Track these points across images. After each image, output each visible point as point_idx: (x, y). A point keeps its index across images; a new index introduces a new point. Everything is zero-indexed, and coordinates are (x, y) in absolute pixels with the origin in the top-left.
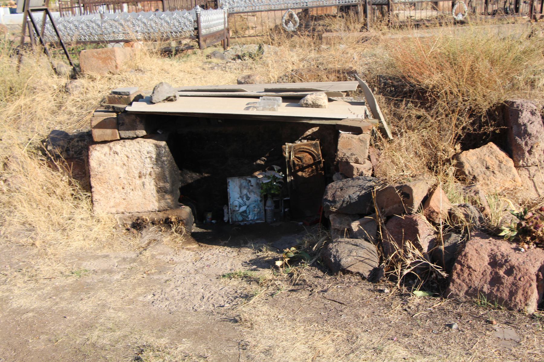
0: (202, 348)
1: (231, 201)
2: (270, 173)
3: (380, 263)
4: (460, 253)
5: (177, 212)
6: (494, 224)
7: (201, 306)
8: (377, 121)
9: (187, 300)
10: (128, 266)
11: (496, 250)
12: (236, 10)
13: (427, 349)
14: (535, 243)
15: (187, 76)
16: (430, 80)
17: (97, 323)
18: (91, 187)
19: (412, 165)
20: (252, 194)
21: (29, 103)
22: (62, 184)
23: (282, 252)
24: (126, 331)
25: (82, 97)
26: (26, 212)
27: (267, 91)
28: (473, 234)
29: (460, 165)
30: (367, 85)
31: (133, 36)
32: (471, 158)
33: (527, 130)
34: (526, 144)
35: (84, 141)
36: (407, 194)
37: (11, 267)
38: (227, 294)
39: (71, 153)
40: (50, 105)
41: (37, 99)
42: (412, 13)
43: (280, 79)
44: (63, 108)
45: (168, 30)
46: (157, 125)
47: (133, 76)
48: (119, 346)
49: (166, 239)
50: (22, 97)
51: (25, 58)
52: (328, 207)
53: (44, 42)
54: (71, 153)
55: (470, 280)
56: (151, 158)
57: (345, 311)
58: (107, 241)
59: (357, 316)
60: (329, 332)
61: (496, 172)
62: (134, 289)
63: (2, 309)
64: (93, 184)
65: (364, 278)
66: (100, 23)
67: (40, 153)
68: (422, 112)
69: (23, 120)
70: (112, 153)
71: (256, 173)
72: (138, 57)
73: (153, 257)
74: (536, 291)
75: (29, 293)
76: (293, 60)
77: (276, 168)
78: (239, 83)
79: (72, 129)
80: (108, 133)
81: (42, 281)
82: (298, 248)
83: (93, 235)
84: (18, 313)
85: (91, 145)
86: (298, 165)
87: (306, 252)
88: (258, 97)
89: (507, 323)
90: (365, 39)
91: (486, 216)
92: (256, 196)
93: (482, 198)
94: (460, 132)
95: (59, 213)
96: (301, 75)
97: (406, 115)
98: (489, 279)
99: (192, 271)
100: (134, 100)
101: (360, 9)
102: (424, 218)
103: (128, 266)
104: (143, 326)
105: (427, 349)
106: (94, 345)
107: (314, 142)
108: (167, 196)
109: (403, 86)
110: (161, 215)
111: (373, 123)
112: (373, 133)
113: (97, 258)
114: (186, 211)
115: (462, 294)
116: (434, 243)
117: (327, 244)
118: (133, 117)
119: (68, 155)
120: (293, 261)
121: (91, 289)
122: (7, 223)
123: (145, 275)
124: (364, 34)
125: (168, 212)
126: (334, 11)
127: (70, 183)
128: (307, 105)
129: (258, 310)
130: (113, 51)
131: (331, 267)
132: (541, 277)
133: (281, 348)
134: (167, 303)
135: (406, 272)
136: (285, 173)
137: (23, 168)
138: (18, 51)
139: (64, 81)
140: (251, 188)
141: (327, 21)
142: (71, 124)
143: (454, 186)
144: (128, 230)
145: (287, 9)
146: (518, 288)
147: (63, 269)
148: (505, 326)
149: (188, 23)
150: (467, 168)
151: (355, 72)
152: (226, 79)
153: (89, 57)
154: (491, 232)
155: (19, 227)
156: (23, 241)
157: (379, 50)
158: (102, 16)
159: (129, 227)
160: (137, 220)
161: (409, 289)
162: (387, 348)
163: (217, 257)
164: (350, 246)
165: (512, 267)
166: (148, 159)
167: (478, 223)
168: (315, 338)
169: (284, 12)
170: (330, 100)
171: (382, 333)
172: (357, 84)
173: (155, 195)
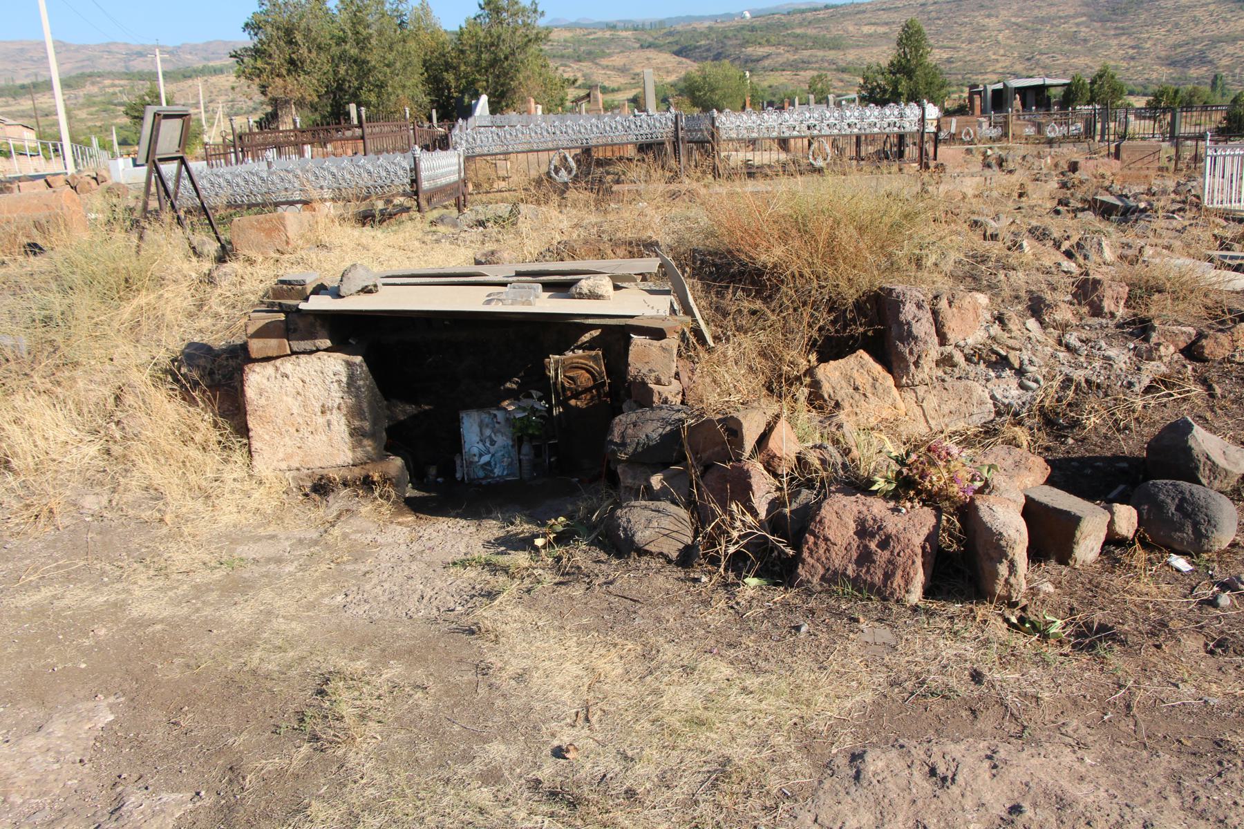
0: (419, 674)
1: (466, 447)
2: (526, 402)
3: (695, 537)
4: (813, 519)
5: (382, 466)
6: (863, 472)
7: (418, 611)
8: (688, 319)
9: (398, 602)
10: (306, 552)
11: (866, 512)
12: (478, 151)
13: (762, 664)
14: (921, 500)
15: (398, 253)
16: (770, 255)
17: (260, 639)
18: (248, 430)
19: (742, 386)
21: (153, 302)
22: (202, 426)
23: (544, 524)
24: (303, 649)
25: (234, 290)
26: (151, 470)
27: (518, 274)
28: (832, 488)
29: (816, 385)
30: (673, 263)
31: (314, 194)
32: (832, 374)
34: (911, 353)
35: (237, 357)
36: (734, 430)
37: (128, 555)
38: (460, 592)
39: (216, 379)
40: (185, 304)
41: (166, 295)
42: (749, 156)
43: (541, 257)
44: (206, 308)
45: (370, 183)
46: (346, 330)
47: (313, 256)
48: (293, 673)
49: (366, 508)
50: (144, 292)
51: (149, 234)
52: (614, 453)
53: (177, 207)
54: (217, 377)
56: (339, 382)
57: (641, 612)
58: (274, 513)
59: (658, 619)
60: (615, 645)
61: (869, 395)
62: (315, 586)
63: (117, 618)
64: (250, 426)
65: (669, 562)
66: (265, 175)
67: (170, 379)
68: (758, 305)
69: (145, 328)
71: (505, 403)
72: (321, 226)
73: (345, 536)
74: (921, 570)
75: (156, 594)
76: (561, 226)
77: (535, 394)
78: (478, 263)
79: (218, 340)
80: (271, 345)
81: (174, 576)
82: (570, 517)
83: (251, 504)
84: (141, 625)
86: (569, 389)
87: (582, 524)
88: (504, 284)
89: (880, 620)
90: (674, 195)
91: (853, 461)
93: (848, 434)
94: (816, 335)
95: (199, 471)
96: (573, 250)
97: (734, 309)
98: (855, 557)
99: (406, 557)
100: (312, 293)
101: (669, 148)
102: (760, 466)
103: (306, 552)
104: (329, 643)
105: (762, 664)
106: (254, 672)
107: (593, 353)
108: (366, 442)
109: (730, 265)
110: (357, 472)
111: (682, 322)
112: (683, 337)
113: (259, 539)
114: (396, 464)
115: (816, 580)
116: (775, 505)
117: (614, 510)
118: (311, 319)
119: (213, 380)
120: (562, 539)
121: (250, 587)
122: (121, 488)
123: (333, 565)
124: (673, 187)
125: (367, 467)
126: (631, 151)
127: (215, 425)
128: (581, 296)
129: (508, 614)
130: (281, 219)
131: (620, 546)
132: (928, 549)
133: (541, 672)
134: (367, 607)
135: (732, 550)
136: (549, 401)
137: (144, 402)
138: (140, 220)
139: (207, 266)
141: (619, 168)
142: (217, 332)
143: (806, 416)
144: (306, 495)
145: (558, 149)
146: (895, 568)
147: (207, 558)
148: (876, 624)
149: (400, 172)
150: (826, 390)
151: (657, 244)
152: (458, 259)
153: (244, 228)
154: (859, 485)
155: (139, 493)
156: (145, 515)
157: (696, 212)
158: (269, 165)
159: (307, 490)
160: (320, 479)
161: (739, 576)
162: (702, 665)
163: (445, 534)
164: (648, 513)
165: (888, 537)
166: (336, 384)
167: (841, 472)
168: (594, 654)
169: (552, 154)
170: (616, 288)
171: (695, 643)
172: (657, 261)
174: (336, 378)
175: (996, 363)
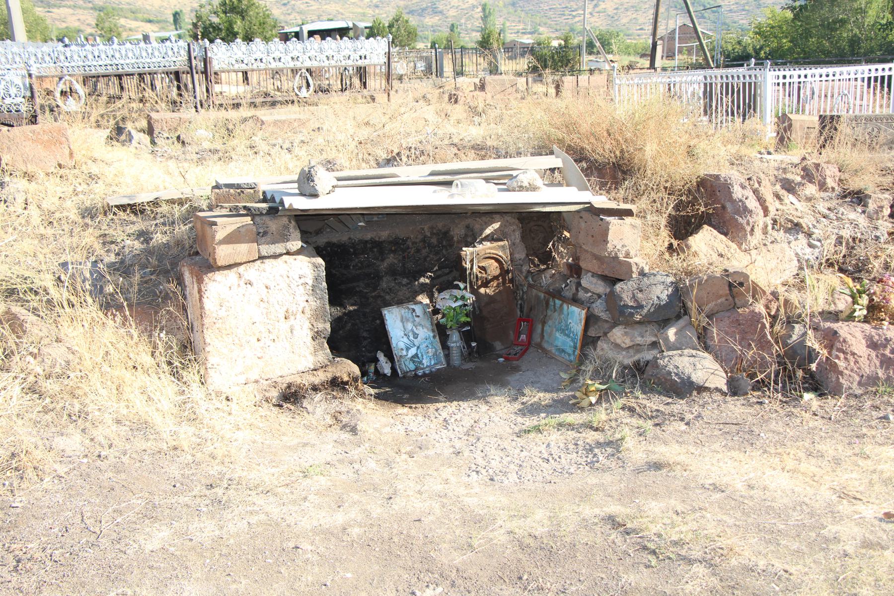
20: (420, 328)
33: (746, 207)
55: (859, 368)
70: (242, 283)
80: (243, 250)
85: (206, 274)
92: (425, 330)
98: (878, 364)
115: (855, 386)
128: (521, 188)
140: (416, 319)
173: (309, 344)
174: (302, 281)
175: (790, 229)
